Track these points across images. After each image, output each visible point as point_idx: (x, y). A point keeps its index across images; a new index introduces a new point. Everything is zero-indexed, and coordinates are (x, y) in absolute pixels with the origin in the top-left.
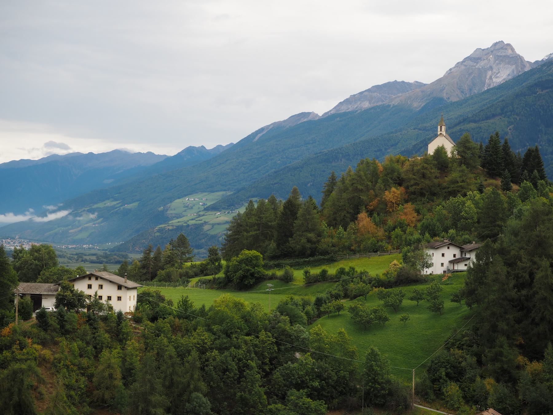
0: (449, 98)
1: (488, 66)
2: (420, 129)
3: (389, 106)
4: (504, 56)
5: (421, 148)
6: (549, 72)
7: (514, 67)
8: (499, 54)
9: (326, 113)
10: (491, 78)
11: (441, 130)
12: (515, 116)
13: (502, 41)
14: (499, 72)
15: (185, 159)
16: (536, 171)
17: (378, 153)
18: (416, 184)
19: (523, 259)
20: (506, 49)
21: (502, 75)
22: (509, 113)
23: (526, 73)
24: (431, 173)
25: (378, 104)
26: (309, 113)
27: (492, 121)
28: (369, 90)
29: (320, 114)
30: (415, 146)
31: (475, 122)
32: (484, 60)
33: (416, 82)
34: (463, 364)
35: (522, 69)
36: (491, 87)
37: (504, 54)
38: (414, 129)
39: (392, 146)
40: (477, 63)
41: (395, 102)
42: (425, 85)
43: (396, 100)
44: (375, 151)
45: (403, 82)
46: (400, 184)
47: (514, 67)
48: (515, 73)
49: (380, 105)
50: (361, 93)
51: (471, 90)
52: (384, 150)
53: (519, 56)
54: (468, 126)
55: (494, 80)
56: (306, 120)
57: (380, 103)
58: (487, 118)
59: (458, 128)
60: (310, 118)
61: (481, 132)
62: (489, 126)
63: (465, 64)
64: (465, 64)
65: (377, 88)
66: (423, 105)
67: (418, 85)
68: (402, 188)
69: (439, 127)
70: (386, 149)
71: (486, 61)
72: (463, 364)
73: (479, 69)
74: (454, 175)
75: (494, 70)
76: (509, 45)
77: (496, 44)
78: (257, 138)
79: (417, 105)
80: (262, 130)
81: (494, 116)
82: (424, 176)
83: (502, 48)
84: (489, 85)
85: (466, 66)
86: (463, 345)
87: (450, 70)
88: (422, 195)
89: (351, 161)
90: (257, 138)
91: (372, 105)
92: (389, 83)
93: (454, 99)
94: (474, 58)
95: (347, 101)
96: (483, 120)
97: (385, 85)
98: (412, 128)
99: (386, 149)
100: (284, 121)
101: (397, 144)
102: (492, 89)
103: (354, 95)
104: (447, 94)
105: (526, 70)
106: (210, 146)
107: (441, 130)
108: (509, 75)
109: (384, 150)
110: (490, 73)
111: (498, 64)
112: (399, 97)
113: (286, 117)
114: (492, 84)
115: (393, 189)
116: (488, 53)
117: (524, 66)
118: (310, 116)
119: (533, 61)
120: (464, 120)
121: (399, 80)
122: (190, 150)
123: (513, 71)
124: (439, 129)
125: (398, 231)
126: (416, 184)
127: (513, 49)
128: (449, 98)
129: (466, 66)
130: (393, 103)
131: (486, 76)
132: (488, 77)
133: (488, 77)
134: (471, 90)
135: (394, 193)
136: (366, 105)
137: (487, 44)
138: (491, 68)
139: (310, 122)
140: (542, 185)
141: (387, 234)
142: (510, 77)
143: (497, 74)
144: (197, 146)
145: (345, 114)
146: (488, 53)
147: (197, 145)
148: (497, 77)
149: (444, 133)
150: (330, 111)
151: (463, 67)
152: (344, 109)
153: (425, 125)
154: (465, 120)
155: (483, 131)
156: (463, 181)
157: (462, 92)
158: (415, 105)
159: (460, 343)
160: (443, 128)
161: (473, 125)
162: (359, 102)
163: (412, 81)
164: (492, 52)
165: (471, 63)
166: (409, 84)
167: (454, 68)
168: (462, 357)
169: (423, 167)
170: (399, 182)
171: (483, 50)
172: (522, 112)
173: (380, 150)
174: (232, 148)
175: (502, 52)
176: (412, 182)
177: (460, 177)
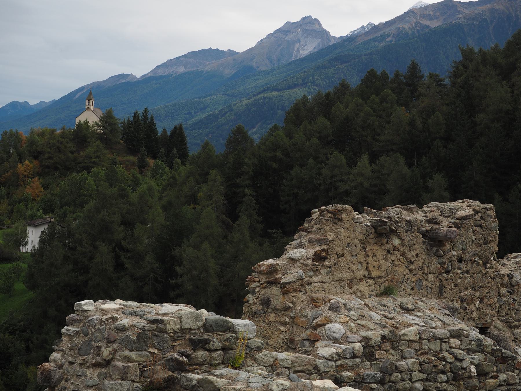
0: (258, 67)
1: (297, 39)
2: (228, 95)
3: (202, 72)
4: (312, 30)
5: (227, 112)
6: (350, 48)
7: (320, 40)
8: (307, 28)
9: (143, 76)
10: (298, 50)
11: (89, 104)
12: (315, 87)
13: (310, 16)
14: (306, 45)
15: (9, 113)
16: (175, 149)
17: (188, 116)
18: (50, 158)
19: (84, 244)
20: (314, 24)
21: (309, 47)
22: (310, 84)
23: (329, 47)
24: (66, 147)
25: (192, 70)
26: (128, 75)
27: (292, 91)
28: (185, 56)
29: (138, 77)
30: (220, 111)
31: (278, 90)
32: (293, 33)
33: (230, 50)
34: (11, 350)
35: (327, 42)
36: (298, 58)
37: (311, 28)
38: (223, 95)
39: (201, 109)
40: (287, 35)
41: (208, 68)
42: (238, 53)
43: (209, 66)
44: (185, 114)
45: (217, 50)
46: (36, 158)
47: (320, 40)
48: (321, 46)
49: (194, 71)
50: (178, 58)
51: (279, 60)
52: (193, 113)
53: (325, 30)
54: (270, 94)
55: (301, 52)
56: (124, 81)
57: (195, 69)
58: (289, 87)
59: (262, 95)
60: (129, 79)
61: (282, 100)
62: (290, 95)
63: (275, 35)
64: (275, 35)
65: (192, 55)
66: (233, 73)
67: (231, 53)
68: (36, 162)
69: (87, 101)
70: (195, 113)
71: (294, 34)
72: (11, 350)
73: (288, 41)
74: (90, 150)
75: (302, 43)
76: (316, 20)
77: (304, 19)
78: (77, 96)
79: (228, 72)
80: (82, 88)
81: (296, 86)
82: (59, 150)
83: (310, 23)
84: (297, 57)
85: (276, 37)
86: (16, 330)
87: (262, 40)
88: (56, 169)
89: (162, 122)
90: (77, 96)
91: (187, 70)
92: (204, 49)
93: (264, 68)
94: (284, 31)
95: (164, 65)
96: (284, 90)
97: (200, 52)
98: (221, 93)
99: (195, 113)
100: (104, 81)
101: (206, 108)
102: (297, 60)
103: (171, 60)
104: (256, 63)
105: (331, 44)
106: (33, 102)
107: (89, 104)
108: (315, 48)
109: (193, 113)
110: (297, 45)
111: (305, 37)
112: (212, 63)
113: (106, 78)
114: (299, 56)
115: (27, 162)
116: (297, 27)
117: (329, 40)
118: (129, 78)
119: (338, 36)
120: (268, 88)
121: (214, 48)
122: (14, 105)
123: (319, 45)
124: (87, 104)
125: (22, 206)
126: (50, 158)
127: (320, 24)
128: (258, 67)
129: (276, 37)
130: (206, 69)
131: (293, 49)
132: (296, 49)
133: (296, 49)
134: (279, 60)
135: (28, 165)
136: (182, 70)
137: (296, 18)
138: (299, 41)
139: (128, 84)
140: (177, 164)
141: (9, 208)
142: (316, 50)
143: (304, 46)
144: (21, 101)
145: (161, 77)
146: (297, 27)
147: (21, 100)
148: (303, 50)
149: (92, 108)
150: (148, 74)
151: (273, 39)
152: (161, 72)
153: (233, 91)
154: (268, 89)
155: (284, 99)
156: (97, 157)
157: (271, 62)
158: (227, 71)
159: (13, 329)
160: (91, 102)
161: (275, 93)
162: (175, 67)
163: (225, 49)
164: (301, 25)
165: (280, 35)
166: (222, 52)
167: (265, 38)
168: (12, 343)
169: (58, 141)
170: (36, 155)
171: (293, 23)
172: (322, 84)
173: (189, 113)
174: (55, 103)
175: (309, 26)
176: (47, 156)
177: (95, 153)
